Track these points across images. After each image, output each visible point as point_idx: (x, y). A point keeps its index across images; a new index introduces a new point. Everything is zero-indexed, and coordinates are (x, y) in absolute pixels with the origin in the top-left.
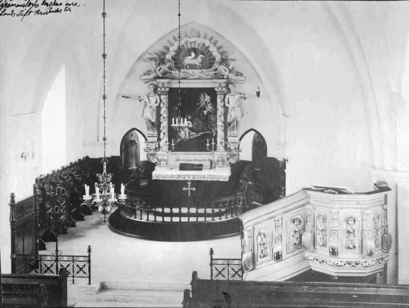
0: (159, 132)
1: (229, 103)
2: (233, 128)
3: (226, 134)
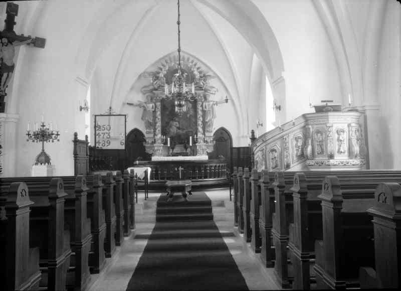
2: (209, 126)
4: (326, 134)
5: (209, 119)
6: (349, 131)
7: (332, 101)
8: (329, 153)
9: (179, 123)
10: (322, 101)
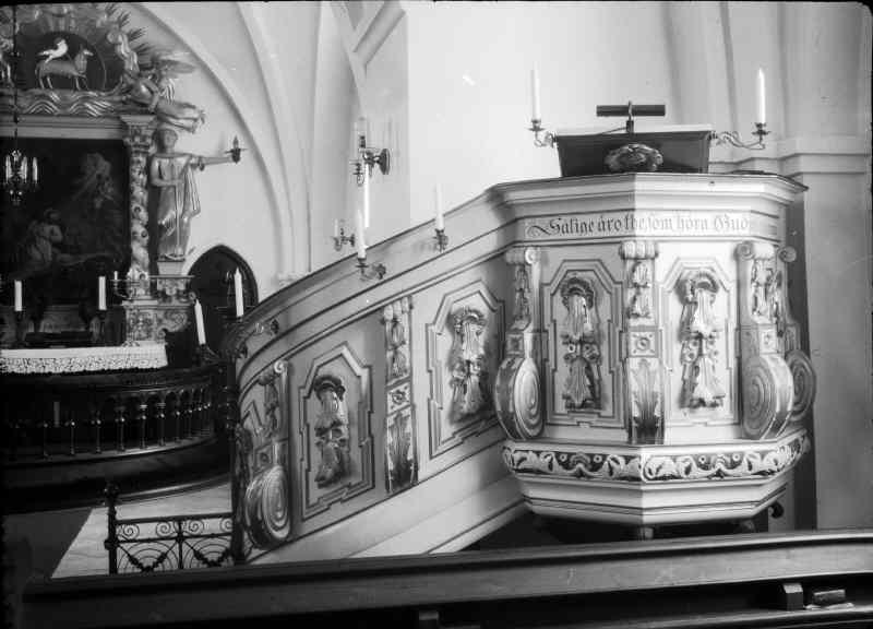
1: (161, 177)
2: (172, 240)
4: (616, 300)
5: (168, 218)
6: (740, 285)
7: (658, 111)
8: (636, 413)
9: (63, 230)
10: (604, 111)
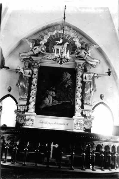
0: (29, 97)
3: (83, 103)
